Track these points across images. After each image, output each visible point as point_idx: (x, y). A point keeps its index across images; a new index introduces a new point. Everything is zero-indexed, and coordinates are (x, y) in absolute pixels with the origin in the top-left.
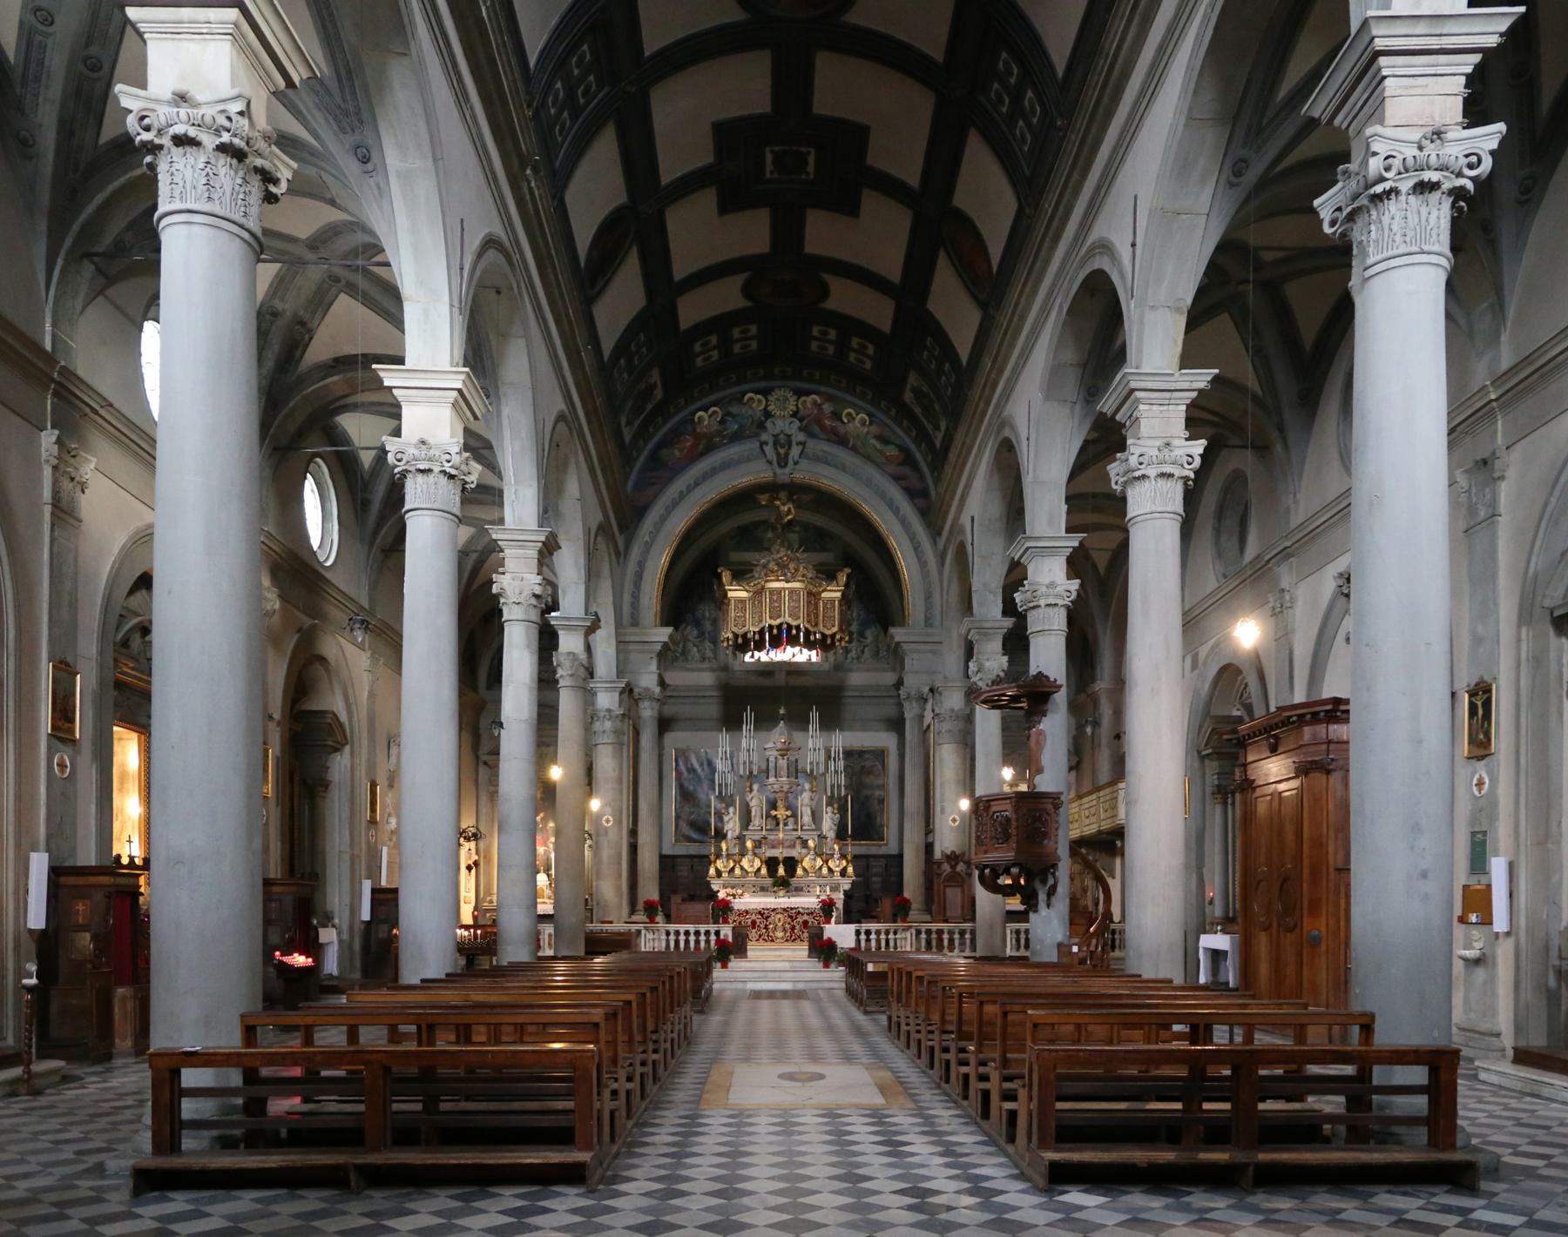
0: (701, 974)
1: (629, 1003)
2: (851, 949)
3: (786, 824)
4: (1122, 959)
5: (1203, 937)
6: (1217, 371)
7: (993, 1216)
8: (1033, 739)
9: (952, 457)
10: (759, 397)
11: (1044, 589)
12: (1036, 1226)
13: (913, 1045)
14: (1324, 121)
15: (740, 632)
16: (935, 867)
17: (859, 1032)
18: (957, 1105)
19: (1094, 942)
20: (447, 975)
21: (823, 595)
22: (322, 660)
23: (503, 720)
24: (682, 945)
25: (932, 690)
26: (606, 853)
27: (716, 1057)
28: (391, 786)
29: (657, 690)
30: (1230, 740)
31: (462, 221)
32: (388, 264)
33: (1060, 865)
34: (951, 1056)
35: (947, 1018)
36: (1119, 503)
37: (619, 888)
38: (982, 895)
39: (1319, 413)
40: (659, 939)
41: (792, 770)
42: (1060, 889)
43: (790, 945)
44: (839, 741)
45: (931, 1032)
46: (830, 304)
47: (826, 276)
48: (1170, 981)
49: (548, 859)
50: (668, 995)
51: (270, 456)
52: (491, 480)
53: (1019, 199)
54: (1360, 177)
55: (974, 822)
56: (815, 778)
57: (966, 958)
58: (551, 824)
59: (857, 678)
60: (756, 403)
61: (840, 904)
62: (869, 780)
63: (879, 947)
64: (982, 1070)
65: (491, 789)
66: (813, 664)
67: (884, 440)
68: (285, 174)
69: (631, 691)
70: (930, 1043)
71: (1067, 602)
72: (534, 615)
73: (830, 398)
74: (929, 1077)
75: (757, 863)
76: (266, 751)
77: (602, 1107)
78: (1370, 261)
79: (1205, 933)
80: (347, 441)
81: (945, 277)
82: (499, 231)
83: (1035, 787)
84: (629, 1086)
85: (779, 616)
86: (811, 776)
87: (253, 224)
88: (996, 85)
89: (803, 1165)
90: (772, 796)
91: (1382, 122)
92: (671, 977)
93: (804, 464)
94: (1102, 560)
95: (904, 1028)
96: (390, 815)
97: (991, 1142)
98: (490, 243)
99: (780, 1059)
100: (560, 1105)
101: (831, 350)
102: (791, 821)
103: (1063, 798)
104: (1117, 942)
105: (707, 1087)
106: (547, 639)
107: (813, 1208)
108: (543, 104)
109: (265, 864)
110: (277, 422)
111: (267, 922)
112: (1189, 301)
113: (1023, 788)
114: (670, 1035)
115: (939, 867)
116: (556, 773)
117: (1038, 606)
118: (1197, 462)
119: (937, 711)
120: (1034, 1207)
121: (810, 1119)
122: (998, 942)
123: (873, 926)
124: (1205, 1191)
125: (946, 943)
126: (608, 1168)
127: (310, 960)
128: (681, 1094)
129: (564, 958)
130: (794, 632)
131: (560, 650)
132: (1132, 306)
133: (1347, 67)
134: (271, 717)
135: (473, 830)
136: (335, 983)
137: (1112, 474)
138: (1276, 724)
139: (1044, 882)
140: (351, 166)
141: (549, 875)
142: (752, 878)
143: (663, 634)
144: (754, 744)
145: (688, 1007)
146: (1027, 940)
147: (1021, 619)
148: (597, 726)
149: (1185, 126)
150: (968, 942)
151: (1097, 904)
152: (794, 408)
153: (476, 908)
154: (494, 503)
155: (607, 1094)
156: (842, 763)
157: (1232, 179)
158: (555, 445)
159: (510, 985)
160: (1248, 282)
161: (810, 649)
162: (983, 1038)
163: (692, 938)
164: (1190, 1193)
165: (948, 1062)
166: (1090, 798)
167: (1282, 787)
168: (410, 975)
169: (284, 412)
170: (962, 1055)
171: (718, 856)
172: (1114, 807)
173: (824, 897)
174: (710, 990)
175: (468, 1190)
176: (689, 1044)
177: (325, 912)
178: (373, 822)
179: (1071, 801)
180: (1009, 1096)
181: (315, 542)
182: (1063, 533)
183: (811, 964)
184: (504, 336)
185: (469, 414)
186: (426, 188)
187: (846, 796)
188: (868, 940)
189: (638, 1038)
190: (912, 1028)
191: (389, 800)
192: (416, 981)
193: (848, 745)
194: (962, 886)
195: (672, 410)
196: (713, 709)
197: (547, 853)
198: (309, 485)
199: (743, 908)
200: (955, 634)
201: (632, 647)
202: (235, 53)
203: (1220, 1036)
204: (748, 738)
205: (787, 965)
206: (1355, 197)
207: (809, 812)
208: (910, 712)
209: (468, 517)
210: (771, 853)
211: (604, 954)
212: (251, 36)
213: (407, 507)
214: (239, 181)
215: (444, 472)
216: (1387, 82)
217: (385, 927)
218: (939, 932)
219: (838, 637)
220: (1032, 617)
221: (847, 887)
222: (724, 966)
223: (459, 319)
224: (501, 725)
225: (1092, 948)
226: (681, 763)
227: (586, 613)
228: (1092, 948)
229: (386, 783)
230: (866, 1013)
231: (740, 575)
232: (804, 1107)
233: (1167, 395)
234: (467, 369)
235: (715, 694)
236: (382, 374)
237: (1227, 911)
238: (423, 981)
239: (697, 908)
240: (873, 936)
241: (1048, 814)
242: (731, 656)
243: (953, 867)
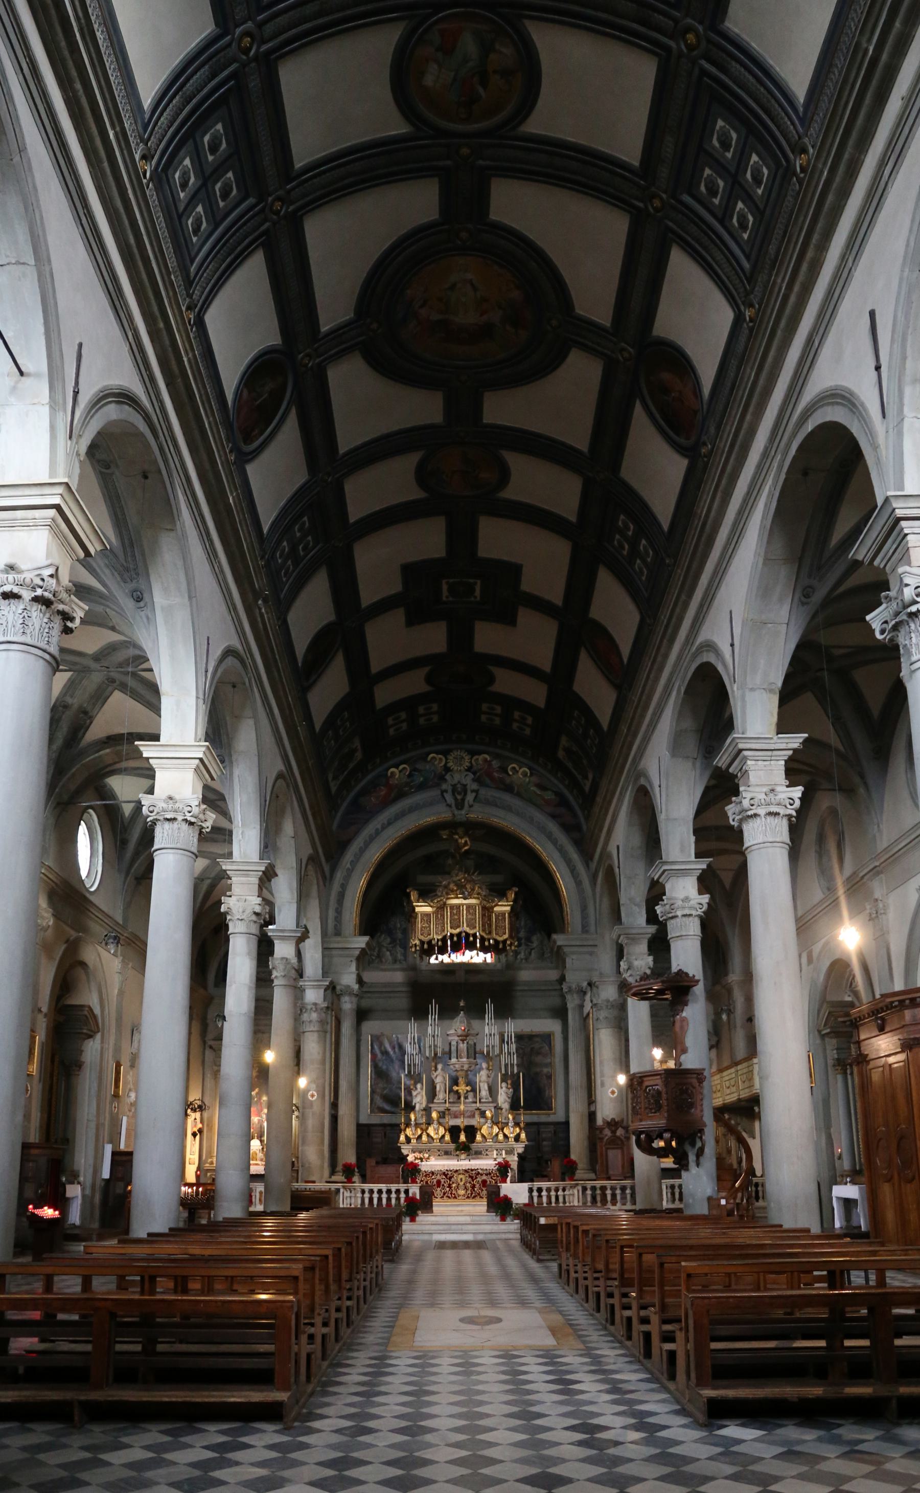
0: (392, 1227)
1: (326, 1257)
2: (525, 1205)
3: (466, 1098)
4: (765, 1208)
5: (835, 1188)
6: (806, 735)
7: (658, 1451)
8: (678, 1025)
9: (599, 799)
10: (440, 756)
11: (680, 903)
12: (698, 1460)
13: (581, 1291)
14: (867, 561)
15: (426, 939)
16: (598, 1132)
17: (534, 1279)
18: (623, 1346)
19: (739, 1195)
20: (171, 1229)
21: (496, 909)
22: (83, 964)
23: (226, 1014)
24: (375, 1201)
25: (590, 984)
26: (311, 1123)
27: (405, 1301)
28: (132, 1066)
29: (356, 987)
30: (844, 1022)
31: (208, 638)
32: (151, 670)
33: (706, 1130)
34: (615, 1301)
35: (611, 1266)
36: (738, 835)
37: (321, 1152)
38: (640, 1159)
39: (890, 765)
40: (355, 1197)
41: (472, 1052)
42: (707, 1150)
43: (470, 1201)
44: (511, 1027)
45: (597, 1279)
46: (497, 687)
47: (491, 668)
48: (808, 1231)
49: (261, 1127)
50: (361, 1247)
51: (55, 808)
52: (224, 823)
53: (641, 613)
54: (899, 601)
55: (630, 1096)
56: (491, 1059)
57: (626, 1211)
58: (265, 1098)
59: (526, 975)
60: (437, 761)
61: (514, 1165)
62: (538, 1059)
63: (549, 1202)
64: (643, 1313)
65: (216, 1068)
66: (488, 964)
67: (543, 788)
68: (79, 614)
69: (334, 988)
70: (596, 1289)
71: (700, 912)
72: (255, 929)
73: (497, 756)
74: (597, 1319)
75: (442, 1131)
76: (33, 1039)
77: (300, 1349)
78: (914, 658)
79: (836, 1184)
80: (111, 795)
82: (236, 643)
83: (681, 1065)
84: (325, 1330)
85: (459, 926)
86: (487, 1057)
87: (54, 650)
88: (617, 537)
89: (481, 1403)
90: (454, 1074)
91: (909, 564)
92: (364, 1233)
93: (477, 807)
94: (727, 879)
95: (573, 1275)
96: (130, 1090)
97: (653, 1379)
98: (229, 652)
99: (462, 1304)
100: (262, 1348)
101: (497, 721)
102: (471, 1095)
103: (706, 1073)
104: (761, 1194)
105: (396, 1330)
107: (491, 1445)
109: (25, 1130)
110: (61, 784)
111: (23, 1179)
112: (779, 684)
113: (671, 1064)
114: (363, 1284)
115: (601, 1132)
116: (269, 1057)
117: (676, 917)
118: (797, 803)
119: (595, 1001)
120: (696, 1441)
121: (487, 1360)
122: (655, 1197)
123: (544, 1185)
124: (854, 1423)
125: (609, 1198)
126: (303, 1407)
127: (57, 1213)
128: (372, 1337)
129: (272, 1214)
130: (471, 939)
131: (275, 956)
132: (735, 689)
133: (878, 527)
134: (40, 1011)
135: (199, 1103)
136: (76, 1232)
137: (730, 814)
138: (882, 1008)
139: (693, 1144)
140: (128, 604)
141: (261, 1141)
142: (437, 1143)
143: (362, 942)
144: (494, 1030)
145: (379, 1257)
146: (681, 1194)
147: (662, 928)
148: (305, 1017)
149: (764, 564)
150: (629, 1197)
151: (740, 1162)
152: (467, 764)
153: (199, 1169)
154: (224, 841)
155: (304, 1338)
156: (514, 1046)
157: (803, 599)
158: (275, 796)
159: (223, 1239)
160: (823, 669)
161: (485, 953)
162: (644, 1283)
163: (384, 1196)
164: (839, 1426)
165: (612, 1306)
166: (729, 1071)
167: (891, 1060)
168: (140, 1230)
169: (67, 776)
170: (625, 1300)
171: (408, 1125)
172: (751, 1079)
173: (500, 1160)
174: (400, 1241)
175: (178, 1425)
176: (380, 1290)
177: (73, 1171)
178: (116, 1096)
179: (712, 1075)
180: (668, 1338)
181: (84, 873)
182: (693, 858)
183: (490, 1218)
184: (238, 717)
185: (207, 776)
186: (182, 616)
187: (518, 1074)
188: (540, 1196)
189: (333, 1287)
190: (580, 1275)
191: (130, 1078)
192: (143, 1235)
193: (518, 1030)
194: (622, 1148)
195: (370, 768)
196: (403, 1002)
197: (260, 1122)
198: (83, 829)
199: (429, 1169)
200: (607, 937)
201: (334, 952)
202: (51, 537)
203: (857, 1278)
205: (468, 1219)
206: (897, 614)
207: (486, 1087)
209: (204, 852)
210: (453, 1122)
211: (307, 1210)
212: (63, 526)
213: (155, 847)
214: (46, 620)
215: (186, 820)
216: (909, 537)
217: (121, 1184)
218: (603, 1188)
219: (508, 942)
220: (671, 925)
221: (521, 1151)
222: (413, 1220)
223: (203, 708)
224: (224, 1018)
225: (738, 1201)
226: (376, 1047)
227: (297, 927)
228: (738, 1201)
229: (129, 1064)
230: (539, 1261)
231: (426, 894)
232: (483, 1348)
233: (769, 753)
234: (207, 744)
235: (404, 989)
236: (142, 749)
237: (854, 1164)
238: (149, 1235)
239: (389, 1170)
240: (544, 1193)
241: (694, 1088)
242: (418, 959)
243: (614, 1132)
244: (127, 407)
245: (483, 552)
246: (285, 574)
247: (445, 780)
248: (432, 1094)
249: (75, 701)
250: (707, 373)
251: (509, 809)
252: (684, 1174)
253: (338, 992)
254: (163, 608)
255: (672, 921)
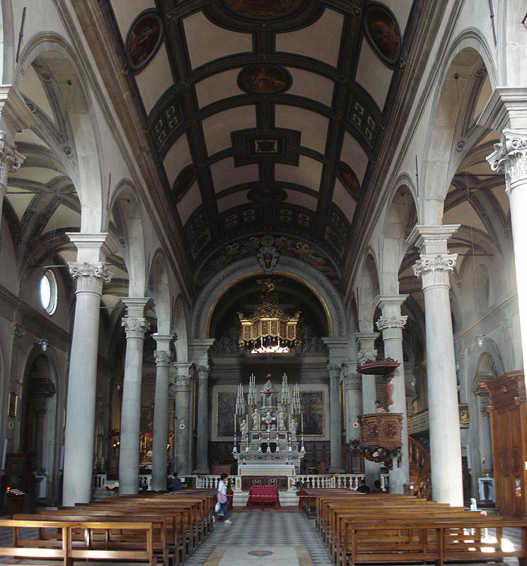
9: (347, 262)
25: (342, 365)
29: (208, 366)
32: (76, 192)
36: (419, 281)
44: (297, 388)
59: (308, 360)
62: (313, 406)
63: (321, 486)
69: (195, 367)
71: (402, 325)
72: (141, 335)
78: (512, 181)
81: (339, 188)
82: (129, 177)
106: (149, 346)
108: (153, 128)
125: (351, 484)
136: (43, 501)
137: (415, 269)
143: (211, 342)
144: (287, 390)
177: (41, 469)
186: (93, 162)
196: (237, 375)
201: (195, 348)
204: (252, 388)
206: (503, 156)
207: (283, 422)
208: (333, 375)
221: (302, 457)
231: (247, 316)
233: (438, 236)
236: (69, 236)
244: (56, 44)
245: (278, 125)
246: (161, 138)
247: (259, 252)
248: (251, 425)
249: (39, 209)
250: (403, 22)
251: (296, 267)
252: (390, 472)
253: (197, 370)
254: (82, 158)
255: (386, 330)
